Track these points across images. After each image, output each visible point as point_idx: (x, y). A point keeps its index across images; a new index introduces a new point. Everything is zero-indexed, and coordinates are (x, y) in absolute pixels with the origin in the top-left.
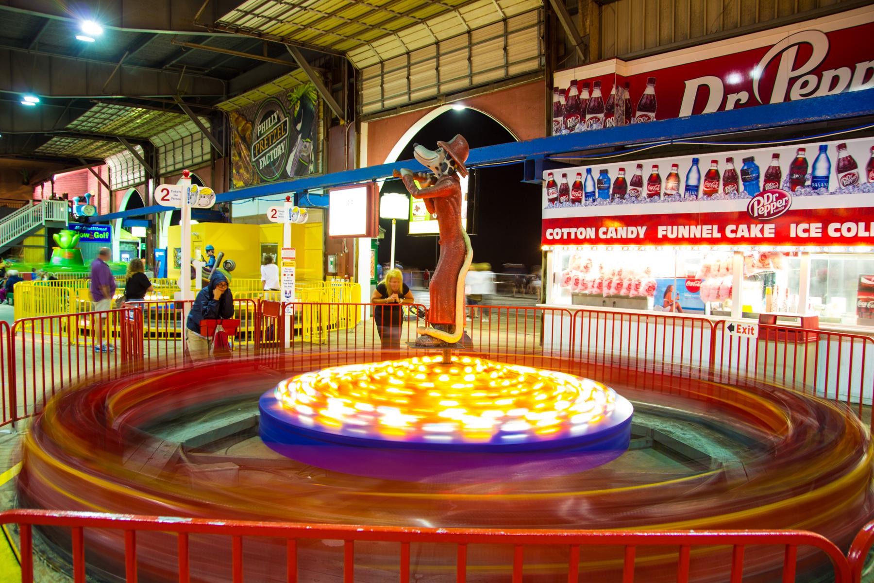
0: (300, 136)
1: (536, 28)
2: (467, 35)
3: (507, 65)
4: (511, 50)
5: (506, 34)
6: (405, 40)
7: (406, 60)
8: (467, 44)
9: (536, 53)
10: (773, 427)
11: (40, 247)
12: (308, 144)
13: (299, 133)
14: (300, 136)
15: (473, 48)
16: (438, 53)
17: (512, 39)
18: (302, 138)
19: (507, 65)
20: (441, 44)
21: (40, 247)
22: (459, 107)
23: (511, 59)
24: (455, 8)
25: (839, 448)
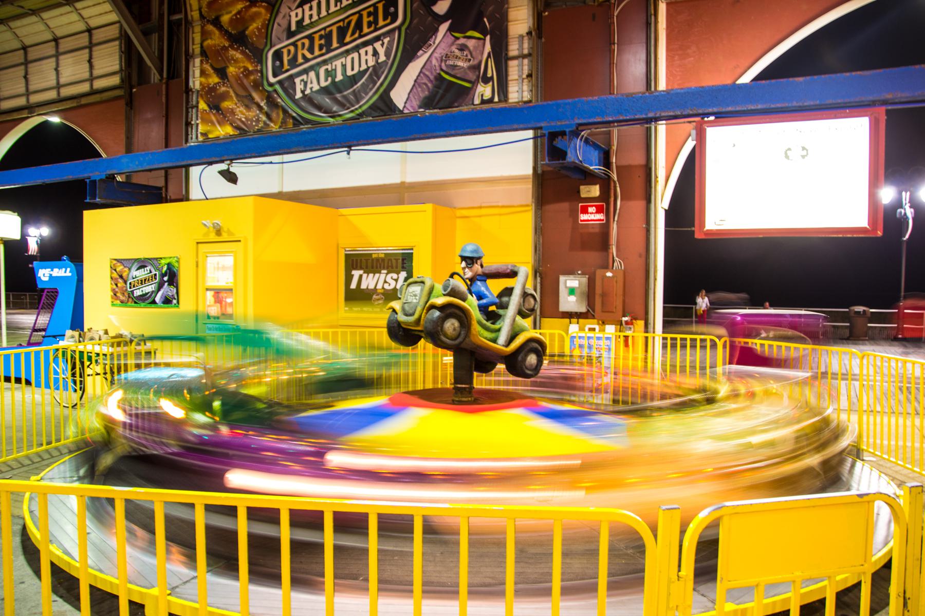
0: (444, 28)
1: (117, 43)
2: (22, 52)
3: (92, 79)
4: (96, 62)
5: (91, 46)
6: (52, 24)
7: (23, 57)
8: (22, 60)
9: (117, 68)
10: (368, 372)
11: (13, 396)
12: (471, 43)
13: (441, 19)
14: (444, 28)
15: (94, 49)
16: (90, 42)
17: (97, 51)
18: (451, 29)
19: (92, 79)
20: (29, 49)
21: (13, 396)
22: (55, 120)
23: (63, 80)
24: (34, 12)
25: (162, 373)
